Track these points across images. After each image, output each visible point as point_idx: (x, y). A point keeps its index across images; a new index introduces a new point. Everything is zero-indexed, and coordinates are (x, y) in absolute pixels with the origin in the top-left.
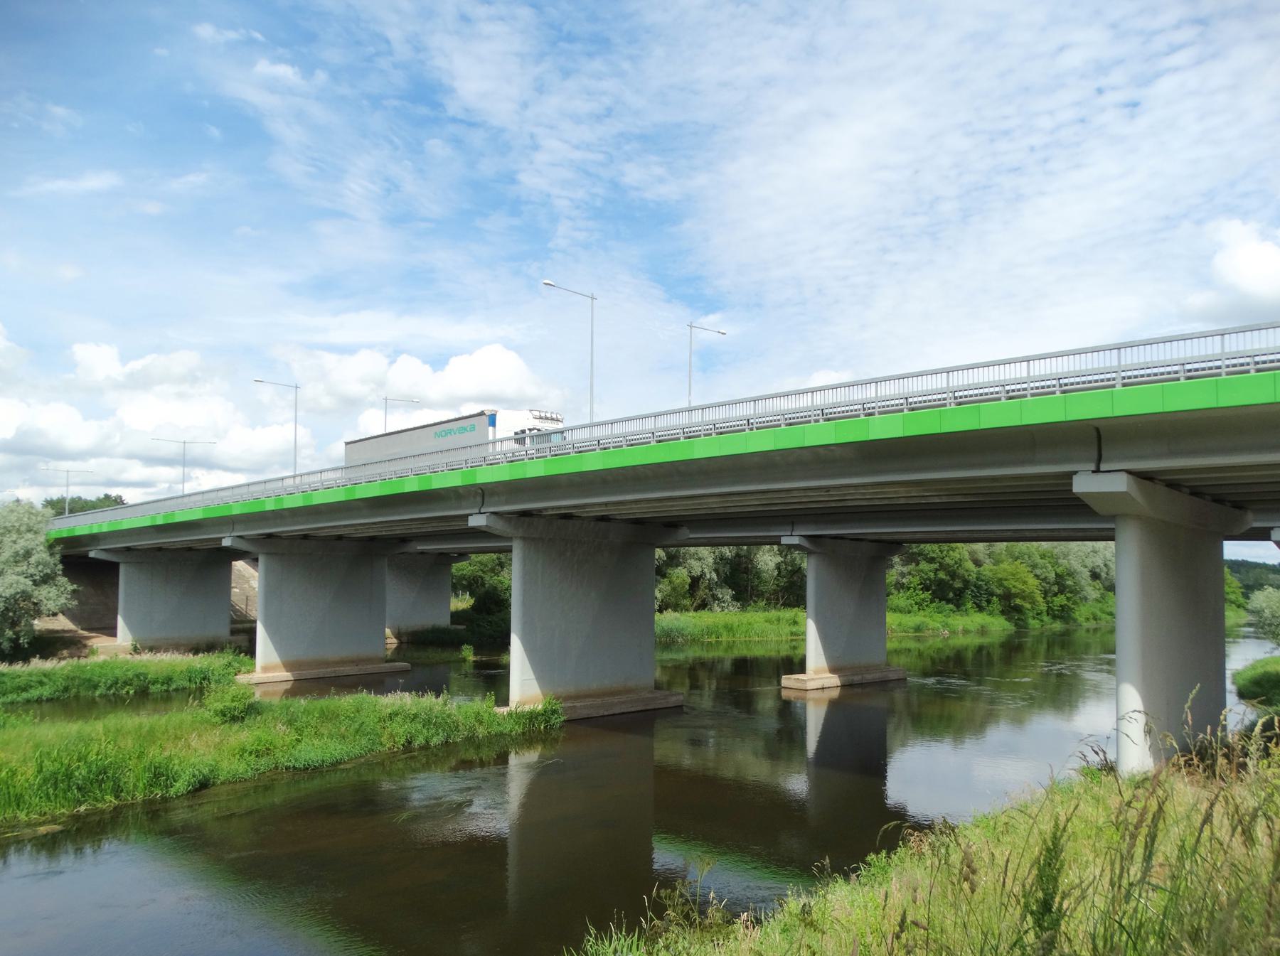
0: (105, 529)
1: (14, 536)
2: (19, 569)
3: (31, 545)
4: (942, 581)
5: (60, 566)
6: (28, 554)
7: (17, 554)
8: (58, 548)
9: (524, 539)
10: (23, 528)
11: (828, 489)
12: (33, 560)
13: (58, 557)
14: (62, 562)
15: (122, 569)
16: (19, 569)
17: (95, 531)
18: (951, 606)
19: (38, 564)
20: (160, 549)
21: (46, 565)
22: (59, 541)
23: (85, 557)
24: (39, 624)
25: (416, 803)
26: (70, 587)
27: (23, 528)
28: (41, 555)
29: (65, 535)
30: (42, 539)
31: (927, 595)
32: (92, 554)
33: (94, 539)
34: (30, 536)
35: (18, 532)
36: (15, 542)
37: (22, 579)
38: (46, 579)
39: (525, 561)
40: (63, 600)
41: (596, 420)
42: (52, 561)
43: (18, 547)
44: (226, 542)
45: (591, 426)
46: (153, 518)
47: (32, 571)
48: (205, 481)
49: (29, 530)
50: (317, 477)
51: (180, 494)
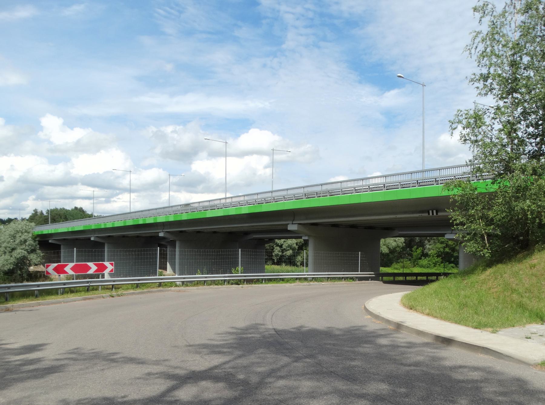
0: (53, 232)
1: (20, 234)
2: (21, 247)
3: (26, 238)
4: (447, 253)
5: (38, 246)
6: (25, 241)
7: (21, 241)
8: (37, 239)
9: (108, 243)
10: (23, 231)
11: (253, 226)
12: (27, 244)
13: (37, 242)
14: (39, 244)
15: (62, 247)
16: (21, 247)
17: (50, 232)
18: (452, 265)
19: (29, 245)
20: (215, 232)
21: (32, 246)
22: (38, 236)
23: (158, 236)
24: (32, 268)
25: (487, 396)
26: (42, 255)
27: (23, 231)
28: (30, 242)
29: (40, 233)
30: (30, 235)
31: (439, 259)
32: (50, 241)
33: (51, 235)
34: (26, 234)
35: (22, 233)
36: (20, 237)
37: (23, 251)
38: (33, 251)
39: (180, 247)
40: (39, 260)
41: (274, 189)
42: (34, 244)
43: (21, 238)
44: (161, 235)
45: (423, 171)
46: (113, 224)
47: (27, 248)
48: (195, 198)
49: (26, 232)
50: (270, 195)
51: (128, 211)
